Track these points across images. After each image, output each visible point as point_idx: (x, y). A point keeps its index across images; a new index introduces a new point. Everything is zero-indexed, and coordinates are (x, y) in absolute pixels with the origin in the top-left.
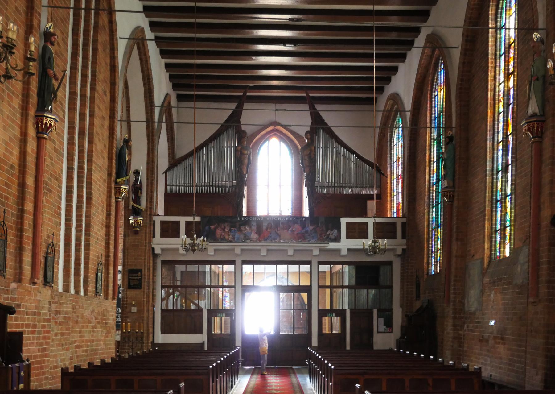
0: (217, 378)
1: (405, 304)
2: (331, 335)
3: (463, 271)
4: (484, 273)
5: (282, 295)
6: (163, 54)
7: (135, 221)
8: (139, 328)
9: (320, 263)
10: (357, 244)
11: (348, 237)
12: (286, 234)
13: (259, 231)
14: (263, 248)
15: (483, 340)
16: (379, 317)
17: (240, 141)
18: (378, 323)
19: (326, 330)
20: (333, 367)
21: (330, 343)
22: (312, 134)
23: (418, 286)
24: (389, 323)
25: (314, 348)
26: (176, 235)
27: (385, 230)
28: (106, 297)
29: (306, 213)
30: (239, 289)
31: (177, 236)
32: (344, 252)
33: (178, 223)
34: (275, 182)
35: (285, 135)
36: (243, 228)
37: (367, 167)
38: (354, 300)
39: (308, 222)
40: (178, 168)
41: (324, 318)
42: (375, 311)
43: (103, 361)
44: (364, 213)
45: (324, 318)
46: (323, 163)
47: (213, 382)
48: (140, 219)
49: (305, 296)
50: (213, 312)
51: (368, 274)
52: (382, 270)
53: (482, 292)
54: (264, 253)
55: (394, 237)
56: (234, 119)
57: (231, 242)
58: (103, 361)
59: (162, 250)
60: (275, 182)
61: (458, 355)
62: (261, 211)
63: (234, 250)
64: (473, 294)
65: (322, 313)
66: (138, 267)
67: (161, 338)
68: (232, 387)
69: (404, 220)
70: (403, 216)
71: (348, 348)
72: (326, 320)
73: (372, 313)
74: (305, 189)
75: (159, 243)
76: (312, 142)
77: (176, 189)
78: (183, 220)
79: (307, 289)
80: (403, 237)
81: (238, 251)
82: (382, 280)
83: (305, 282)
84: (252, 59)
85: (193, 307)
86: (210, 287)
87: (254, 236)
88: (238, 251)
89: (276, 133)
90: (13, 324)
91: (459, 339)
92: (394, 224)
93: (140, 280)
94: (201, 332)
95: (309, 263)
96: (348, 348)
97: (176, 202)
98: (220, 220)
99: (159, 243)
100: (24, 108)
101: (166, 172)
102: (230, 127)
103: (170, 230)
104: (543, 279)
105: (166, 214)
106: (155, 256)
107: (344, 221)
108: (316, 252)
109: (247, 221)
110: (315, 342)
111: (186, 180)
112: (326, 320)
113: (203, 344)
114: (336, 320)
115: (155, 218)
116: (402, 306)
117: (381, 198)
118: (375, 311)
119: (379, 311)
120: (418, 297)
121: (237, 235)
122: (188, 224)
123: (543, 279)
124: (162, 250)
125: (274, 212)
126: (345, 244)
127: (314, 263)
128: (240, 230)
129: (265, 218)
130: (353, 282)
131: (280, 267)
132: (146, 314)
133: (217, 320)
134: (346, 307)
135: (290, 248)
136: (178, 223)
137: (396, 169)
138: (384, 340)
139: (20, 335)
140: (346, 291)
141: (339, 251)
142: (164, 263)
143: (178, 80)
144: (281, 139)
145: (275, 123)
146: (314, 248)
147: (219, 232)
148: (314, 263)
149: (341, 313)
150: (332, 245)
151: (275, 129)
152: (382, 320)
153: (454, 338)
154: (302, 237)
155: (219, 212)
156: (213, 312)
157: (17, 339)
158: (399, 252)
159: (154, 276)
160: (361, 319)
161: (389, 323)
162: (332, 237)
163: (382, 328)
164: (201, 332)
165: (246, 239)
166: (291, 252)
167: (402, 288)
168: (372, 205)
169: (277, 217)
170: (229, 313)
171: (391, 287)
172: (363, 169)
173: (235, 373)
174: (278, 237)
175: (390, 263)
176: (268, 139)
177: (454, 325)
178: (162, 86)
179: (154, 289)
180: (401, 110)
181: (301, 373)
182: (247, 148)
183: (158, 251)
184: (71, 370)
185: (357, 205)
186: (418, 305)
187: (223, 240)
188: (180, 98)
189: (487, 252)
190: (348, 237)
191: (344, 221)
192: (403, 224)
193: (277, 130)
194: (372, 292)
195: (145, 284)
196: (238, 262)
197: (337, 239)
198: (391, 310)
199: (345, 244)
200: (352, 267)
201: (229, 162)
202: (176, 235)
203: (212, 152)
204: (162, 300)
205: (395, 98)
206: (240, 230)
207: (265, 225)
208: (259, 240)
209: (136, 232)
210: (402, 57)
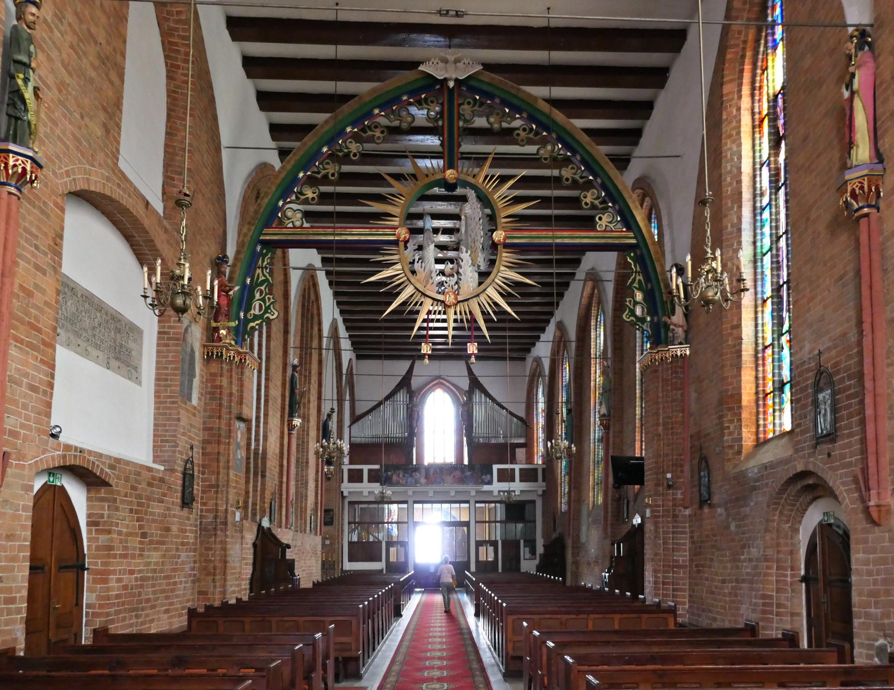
0: (369, 618)
1: (545, 535)
2: (487, 562)
3: (578, 512)
4: (589, 514)
5: (447, 529)
6: (348, 329)
7: (329, 470)
8: (332, 557)
9: (477, 502)
10: (505, 486)
11: (499, 481)
12: (449, 479)
13: (427, 477)
14: (431, 490)
15: (589, 564)
16: (525, 547)
17: (411, 398)
18: (524, 552)
19: (482, 558)
20: (504, 605)
21: (484, 567)
22: (470, 393)
23: (555, 521)
24: (533, 552)
25: (472, 573)
26: (360, 480)
27: (528, 475)
28: (316, 535)
29: (466, 462)
30: (411, 523)
31: (361, 481)
32: (496, 493)
33: (362, 470)
34: (439, 431)
35: (448, 387)
36: (414, 474)
37: (515, 419)
38: (505, 532)
39: (466, 469)
40: (360, 422)
41: (480, 548)
42: (522, 542)
43: (239, 600)
44: (513, 461)
45: (480, 548)
46: (480, 412)
47: (364, 623)
48: (332, 468)
49: (465, 528)
50: (390, 544)
51: (516, 510)
52: (527, 507)
53: (588, 528)
54: (431, 494)
55: (536, 480)
56: (405, 382)
57: (404, 486)
58: (239, 600)
59: (349, 493)
60: (439, 431)
61: (577, 576)
62: (428, 460)
63: (407, 492)
64: (584, 528)
65: (479, 544)
66: (331, 508)
67: (348, 566)
68: (374, 650)
69: (544, 466)
70: (543, 463)
71: (500, 570)
72: (482, 549)
73: (519, 542)
74: (465, 439)
75: (347, 487)
76: (470, 399)
77: (358, 440)
78: (366, 468)
79: (467, 524)
80: (544, 481)
81: (410, 493)
82: (527, 515)
83: (465, 518)
84: (396, 141)
85: (371, 539)
86: (388, 523)
87: (423, 480)
88: (410, 493)
89: (440, 385)
90: (289, 555)
91: (576, 563)
92: (535, 470)
93: (332, 518)
94: (381, 560)
95: (467, 502)
96: (500, 570)
97: (359, 451)
98: (396, 468)
99: (347, 487)
100: (282, 416)
101: (350, 426)
102: (402, 388)
103: (355, 477)
104: (609, 522)
105: (351, 463)
106: (343, 497)
107: (495, 467)
108: (473, 493)
109: (416, 469)
110: (473, 568)
111: (366, 431)
112: (482, 549)
113: (382, 570)
114: (491, 549)
115: (343, 467)
116: (543, 537)
117: (528, 446)
118: (522, 542)
119: (525, 541)
120: (555, 529)
121: (409, 480)
122: (370, 471)
123: (609, 522)
124: (349, 493)
125: (439, 460)
126: (497, 487)
127: (472, 502)
128: (411, 476)
129: (431, 466)
130: (504, 518)
131: (444, 505)
132: (337, 546)
133: (393, 550)
134: (498, 538)
135: (453, 489)
136: (362, 470)
137: (540, 421)
138: (529, 566)
139: (293, 561)
140: (498, 525)
141: (491, 492)
142: (350, 503)
143: (356, 345)
144: (445, 391)
145: (439, 377)
146: (472, 489)
147: (395, 478)
148: (472, 502)
149: (494, 544)
150: (486, 488)
151: (438, 381)
152: (527, 549)
153: (573, 562)
154: (462, 481)
155: (394, 460)
156: (390, 544)
157: (291, 564)
158: (540, 492)
159: (342, 514)
160: (511, 549)
161: (533, 552)
162: (486, 481)
163: (528, 555)
164: (381, 560)
165: (417, 482)
166: (453, 494)
167: (543, 523)
168: (520, 453)
169: (442, 464)
170: (403, 544)
171: (535, 521)
172: (511, 421)
173: (410, 592)
174: (442, 481)
175: (533, 502)
176: (434, 391)
177: (573, 553)
178: (347, 355)
179: (342, 525)
180: (541, 375)
181: (461, 592)
182: (416, 406)
183: (345, 494)
184: (201, 610)
185: (505, 452)
186: (554, 536)
187: (398, 484)
188: (359, 357)
189: (591, 499)
190: (499, 481)
191: (495, 467)
192: (544, 470)
193: (442, 383)
194: (520, 526)
195: (336, 522)
196: (410, 502)
197: (490, 483)
198: (535, 541)
199: (497, 487)
200: (503, 506)
201: (402, 414)
202: (360, 480)
203: (387, 408)
204: (349, 536)
205: (538, 361)
206: (411, 476)
207: (432, 471)
208: (427, 484)
209: (329, 479)
210: (543, 330)
